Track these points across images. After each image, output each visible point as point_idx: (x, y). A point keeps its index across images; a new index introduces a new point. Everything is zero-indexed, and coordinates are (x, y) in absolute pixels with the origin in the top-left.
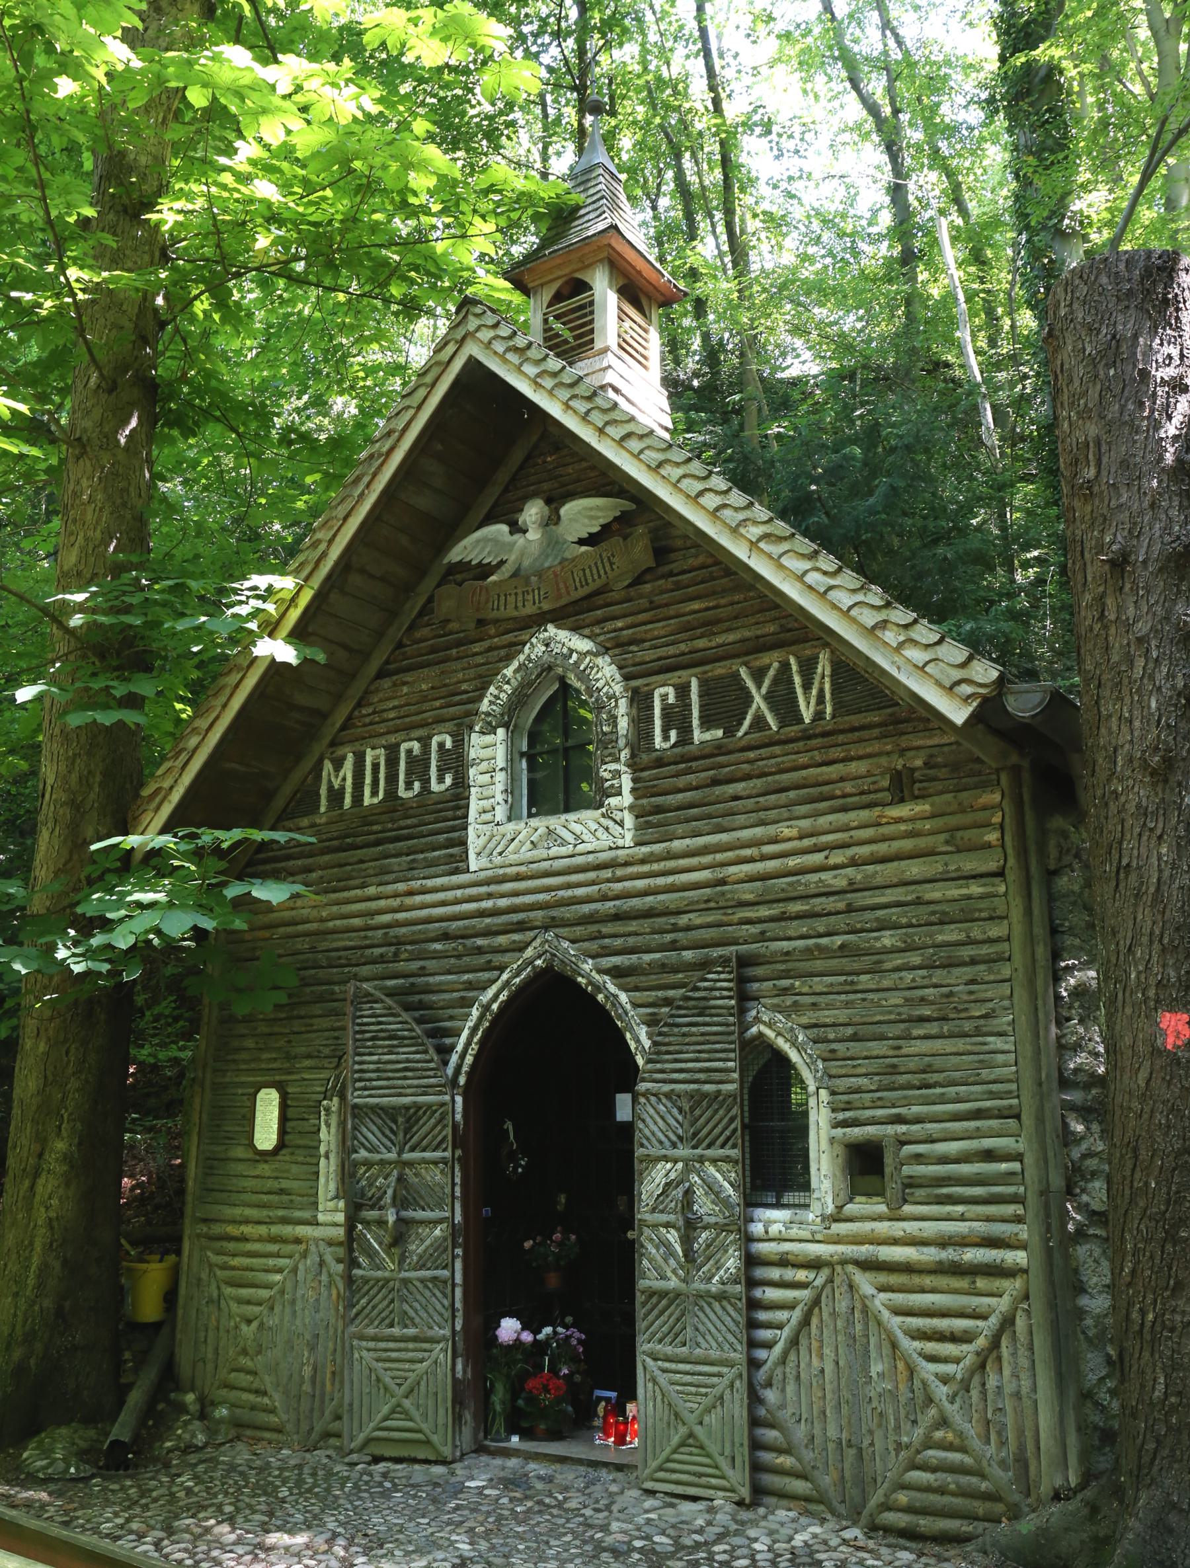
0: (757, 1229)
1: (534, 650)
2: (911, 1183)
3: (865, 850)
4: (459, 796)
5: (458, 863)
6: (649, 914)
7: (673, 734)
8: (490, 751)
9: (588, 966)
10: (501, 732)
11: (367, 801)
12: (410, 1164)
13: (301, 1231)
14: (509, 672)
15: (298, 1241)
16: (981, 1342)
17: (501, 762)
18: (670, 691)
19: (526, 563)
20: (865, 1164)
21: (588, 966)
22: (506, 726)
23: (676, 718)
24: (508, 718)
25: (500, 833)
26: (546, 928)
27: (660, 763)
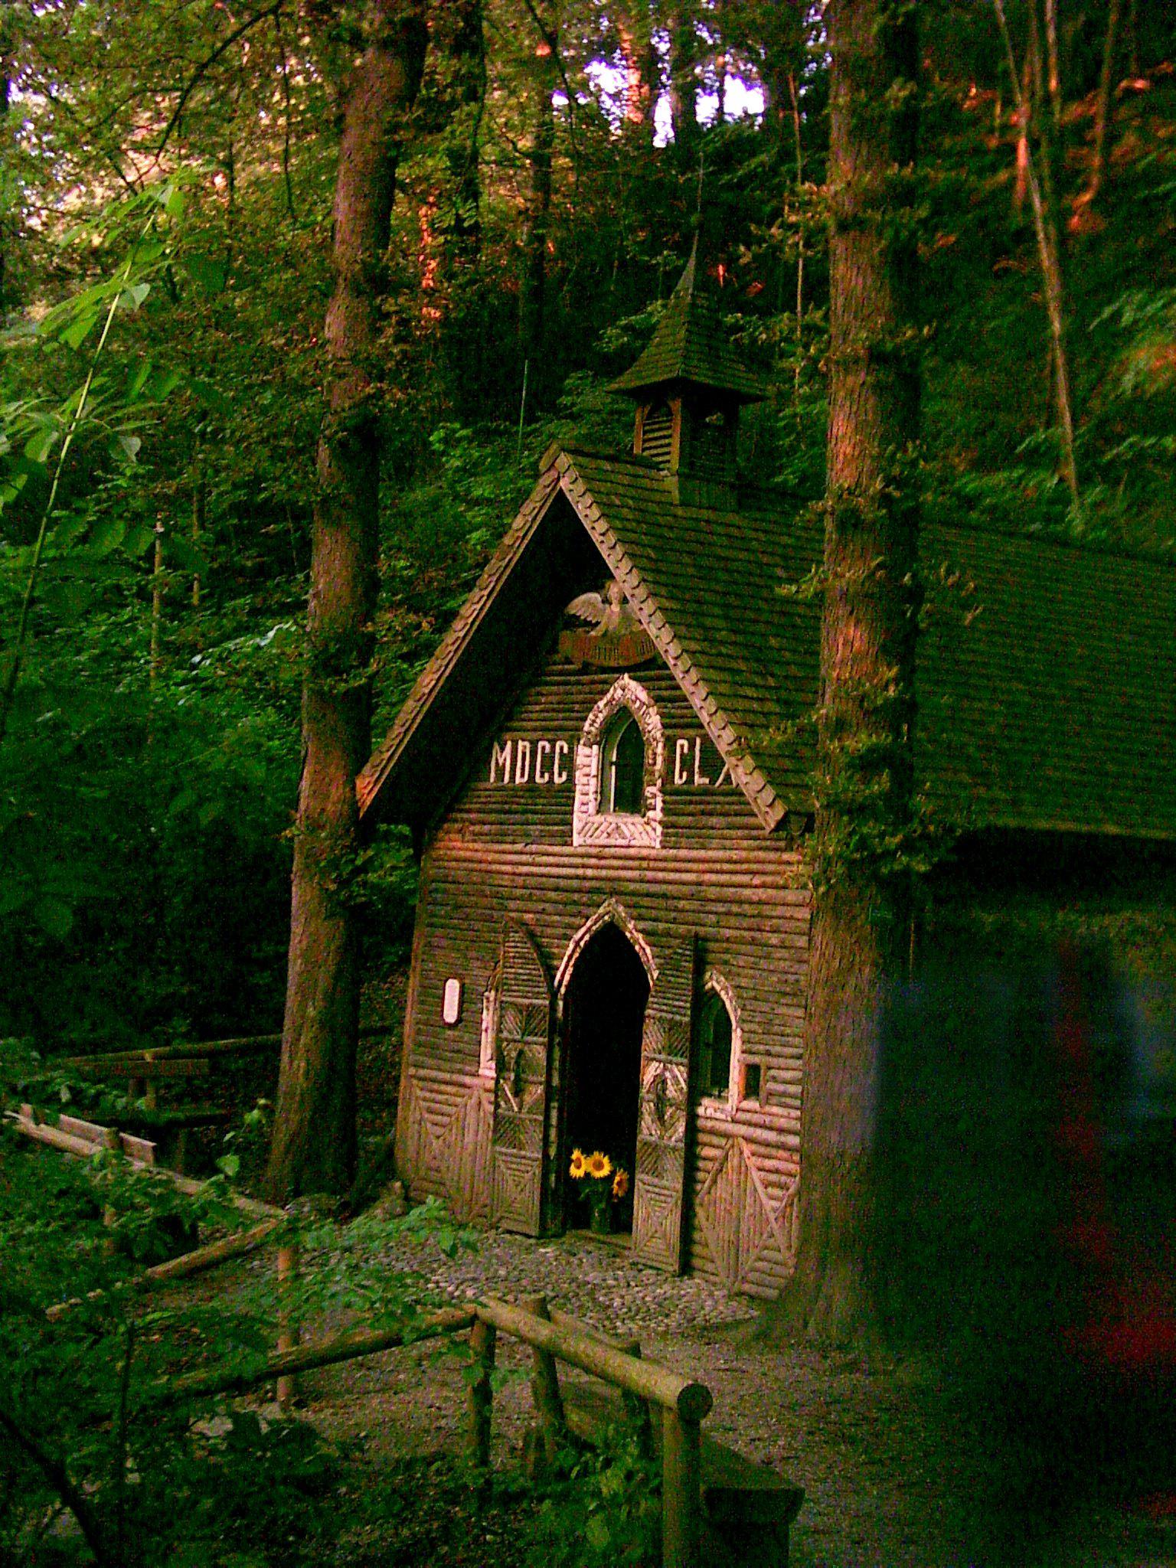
0: (700, 1111)
1: (615, 693)
2: (770, 1094)
3: (769, 879)
4: (569, 787)
5: (566, 838)
6: (664, 896)
8: (587, 757)
11: (518, 780)
12: (528, 1043)
13: (468, 1080)
14: (601, 704)
15: (464, 1086)
17: (594, 772)
18: (685, 743)
21: (630, 926)
22: (598, 743)
23: (687, 765)
25: (591, 824)
26: (611, 894)
27: (677, 792)
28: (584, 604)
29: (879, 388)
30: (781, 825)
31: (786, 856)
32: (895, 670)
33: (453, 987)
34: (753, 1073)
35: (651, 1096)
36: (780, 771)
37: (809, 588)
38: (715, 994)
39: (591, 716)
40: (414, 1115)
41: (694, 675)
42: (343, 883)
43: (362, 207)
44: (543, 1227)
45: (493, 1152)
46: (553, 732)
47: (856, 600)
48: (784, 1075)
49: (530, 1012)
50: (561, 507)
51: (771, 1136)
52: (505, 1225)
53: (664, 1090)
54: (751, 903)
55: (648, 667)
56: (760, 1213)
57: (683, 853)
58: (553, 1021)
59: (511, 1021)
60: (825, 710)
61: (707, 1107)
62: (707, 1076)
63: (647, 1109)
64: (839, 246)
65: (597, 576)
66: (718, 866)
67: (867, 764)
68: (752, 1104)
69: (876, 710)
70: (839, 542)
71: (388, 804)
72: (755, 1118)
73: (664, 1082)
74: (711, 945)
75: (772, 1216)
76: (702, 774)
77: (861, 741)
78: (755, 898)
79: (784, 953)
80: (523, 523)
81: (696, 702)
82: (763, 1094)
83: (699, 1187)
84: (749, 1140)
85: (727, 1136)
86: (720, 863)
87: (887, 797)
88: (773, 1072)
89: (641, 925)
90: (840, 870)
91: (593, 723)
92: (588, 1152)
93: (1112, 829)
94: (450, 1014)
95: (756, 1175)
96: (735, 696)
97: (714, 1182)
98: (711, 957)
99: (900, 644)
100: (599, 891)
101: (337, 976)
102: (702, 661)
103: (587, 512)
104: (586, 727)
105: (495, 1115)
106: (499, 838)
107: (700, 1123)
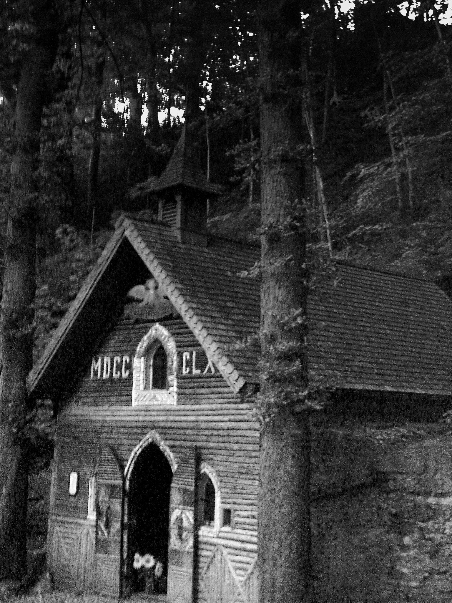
3: (232, 418)
5: (129, 402)
7: (188, 369)
8: (139, 364)
9: (162, 443)
10: (143, 358)
16: (249, 572)
17: (142, 370)
19: (150, 301)
20: (227, 516)
21: (162, 443)
23: (189, 364)
24: (146, 353)
27: (184, 378)
28: (136, 291)
29: (285, 174)
30: (242, 390)
31: (241, 406)
32: (300, 310)
33: (73, 477)
34: (227, 513)
35: (176, 526)
36: (244, 362)
37: (255, 272)
38: (206, 475)
39: (140, 343)
40: (55, 540)
41: (195, 319)
42: (19, 429)
43: (28, 113)
44: (121, 593)
45: (96, 558)
46: (121, 353)
47: (278, 278)
48: (243, 513)
49: (112, 488)
50: (126, 246)
51: (238, 545)
52: (103, 592)
53: (182, 522)
54: (223, 430)
55: (171, 319)
56: (233, 584)
57: (188, 407)
58: (124, 491)
59: (103, 493)
60: (265, 330)
61: (204, 531)
62: (205, 515)
63: (174, 533)
64: (265, 108)
65: (143, 275)
66: (206, 413)
67: (287, 357)
68: (227, 528)
69: (290, 330)
70: (269, 250)
71: (41, 391)
72: (229, 535)
73: (181, 520)
74: (203, 451)
75: (239, 586)
76: (197, 368)
77: (283, 346)
78: (226, 427)
79: (242, 453)
80: (108, 253)
81: (196, 332)
82: (232, 524)
83: (200, 570)
84: (227, 547)
85: (214, 545)
86: (209, 411)
87: (297, 373)
88: (237, 513)
89: (168, 443)
90: (276, 410)
91: (141, 347)
92: (142, 554)
93: (389, 389)
94: (73, 489)
95: (230, 565)
96: (216, 329)
97: (208, 568)
98: (203, 457)
99: (301, 296)
100: (144, 428)
101: (18, 474)
102: (200, 313)
103: (139, 246)
104: (138, 349)
105: (96, 538)
106: (96, 404)
107: (200, 539)
